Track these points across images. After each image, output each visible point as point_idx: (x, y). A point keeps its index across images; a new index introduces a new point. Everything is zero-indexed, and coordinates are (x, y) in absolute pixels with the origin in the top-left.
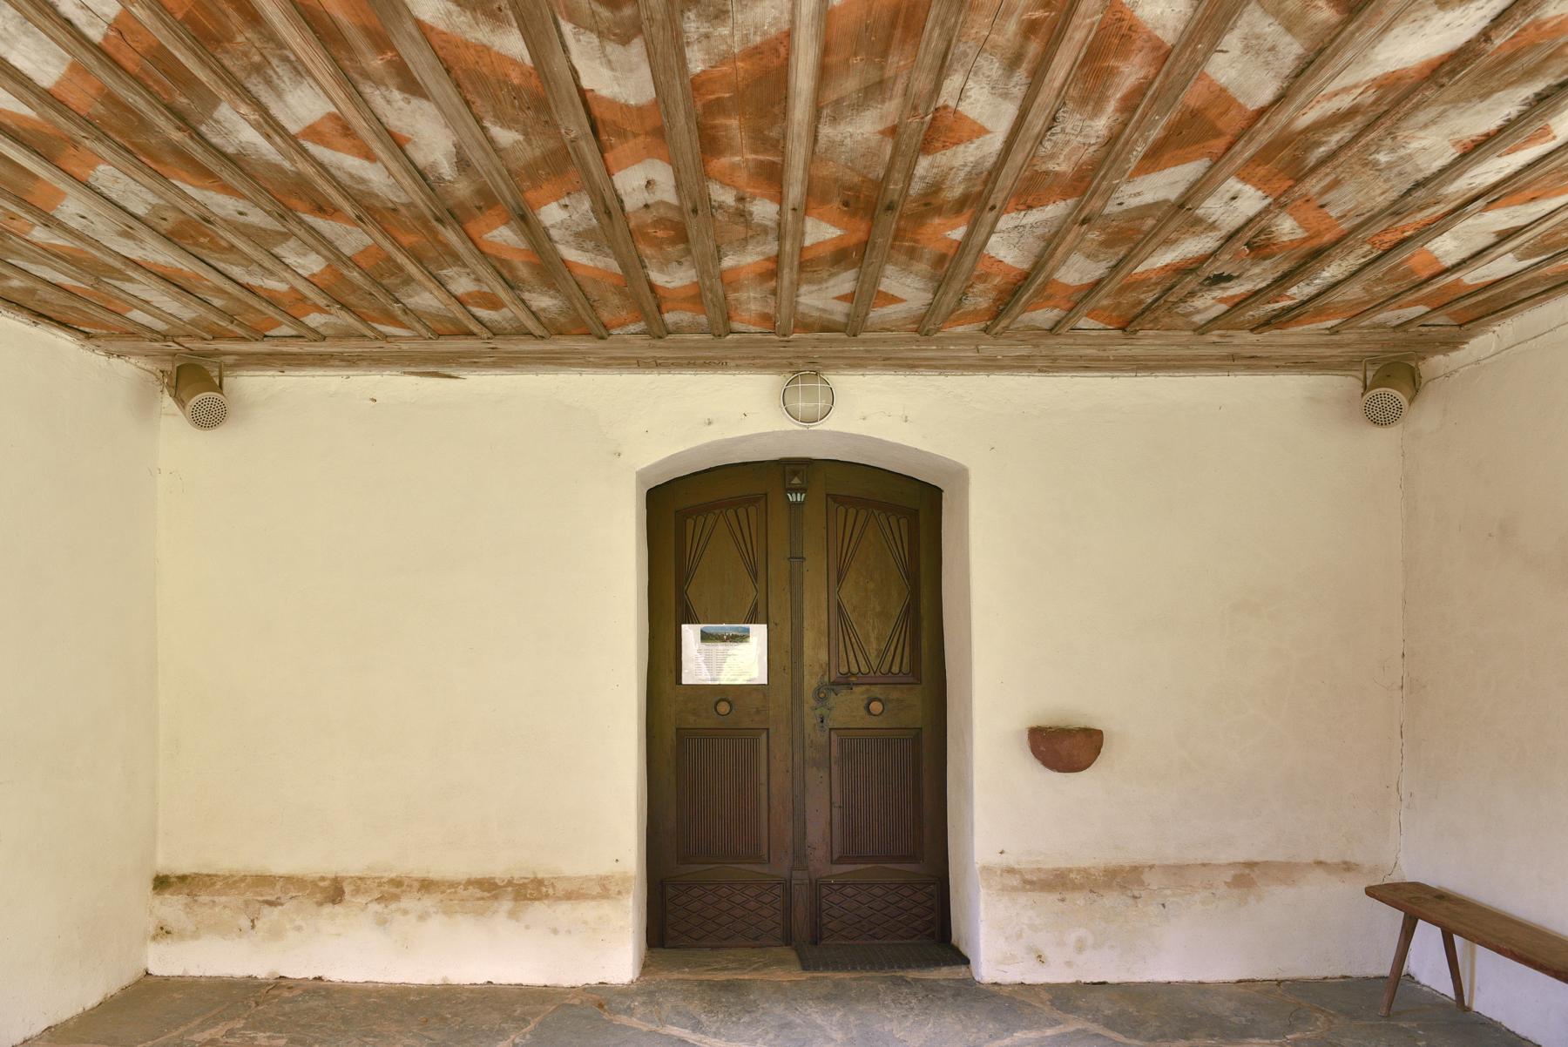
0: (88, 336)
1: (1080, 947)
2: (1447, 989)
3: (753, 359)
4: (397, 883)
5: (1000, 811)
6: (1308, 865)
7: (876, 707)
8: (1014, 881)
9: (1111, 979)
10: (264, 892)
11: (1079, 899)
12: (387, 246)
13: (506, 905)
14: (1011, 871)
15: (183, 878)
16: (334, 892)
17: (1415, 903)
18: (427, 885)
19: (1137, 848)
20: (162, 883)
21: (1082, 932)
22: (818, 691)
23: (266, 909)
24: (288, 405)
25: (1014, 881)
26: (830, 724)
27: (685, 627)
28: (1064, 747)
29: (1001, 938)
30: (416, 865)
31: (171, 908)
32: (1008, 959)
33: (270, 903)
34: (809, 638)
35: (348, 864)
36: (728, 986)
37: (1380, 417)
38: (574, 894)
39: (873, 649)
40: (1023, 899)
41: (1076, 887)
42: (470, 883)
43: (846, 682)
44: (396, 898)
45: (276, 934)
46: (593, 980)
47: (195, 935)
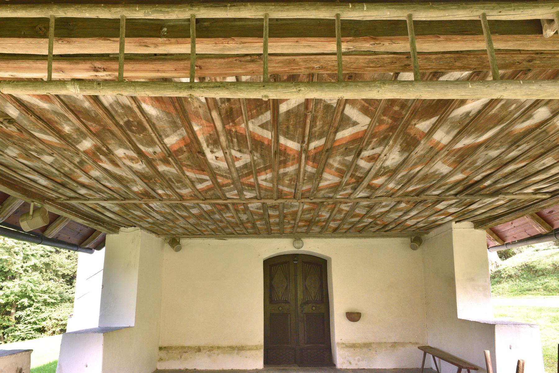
0: (158, 234)
1: (359, 361)
2: (434, 368)
3: (287, 236)
4: (212, 347)
5: (341, 331)
6: (407, 343)
7: (314, 308)
8: (344, 346)
9: (366, 368)
10: (184, 350)
11: (358, 350)
12: (181, 175)
13: (236, 351)
14: (343, 344)
15: (165, 347)
16: (199, 349)
17: (426, 350)
18: (219, 348)
19: (371, 339)
20: (161, 349)
21: (359, 357)
22: (301, 305)
23: (184, 354)
24: (193, 246)
25: (344, 346)
26: (304, 312)
27: (461, 315)
28: (353, 316)
29: (341, 358)
30: (216, 344)
31: (163, 354)
32: (343, 363)
33: (185, 352)
34: (299, 292)
35: (201, 342)
36: (284, 369)
37: (414, 248)
38: (251, 349)
39: (313, 295)
40: (346, 349)
41: (357, 347)
42: (228, 347)
43: (306, 303)
44: (212, 350)
45: (186, 359)
46: (254, 368)
47: (168, 360)
